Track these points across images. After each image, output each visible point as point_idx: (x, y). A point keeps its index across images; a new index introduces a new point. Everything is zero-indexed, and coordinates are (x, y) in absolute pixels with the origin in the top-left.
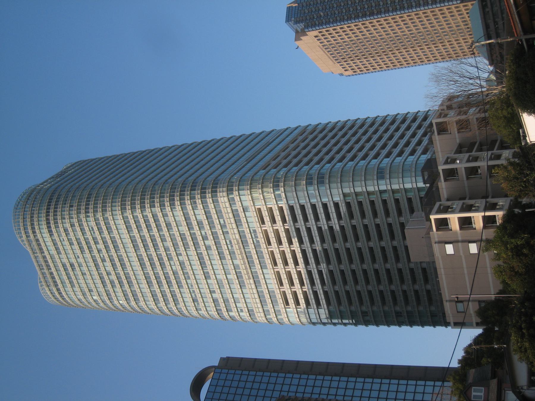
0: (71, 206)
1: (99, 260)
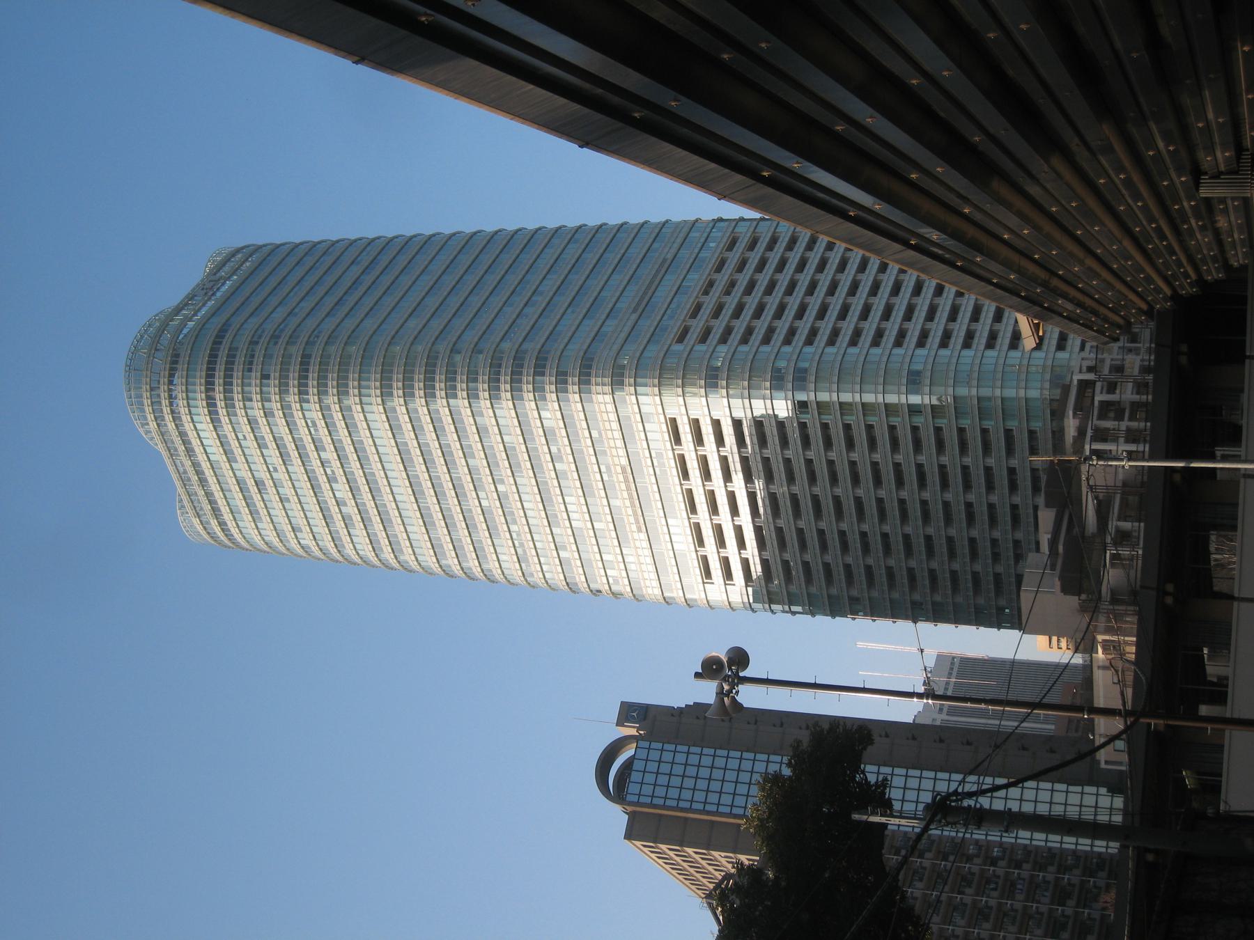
0: (265, 377)
1: (322, 479)
